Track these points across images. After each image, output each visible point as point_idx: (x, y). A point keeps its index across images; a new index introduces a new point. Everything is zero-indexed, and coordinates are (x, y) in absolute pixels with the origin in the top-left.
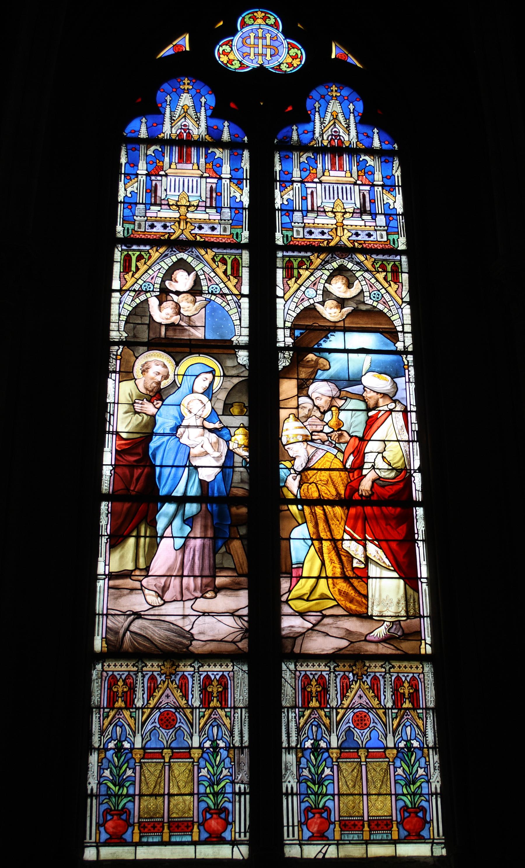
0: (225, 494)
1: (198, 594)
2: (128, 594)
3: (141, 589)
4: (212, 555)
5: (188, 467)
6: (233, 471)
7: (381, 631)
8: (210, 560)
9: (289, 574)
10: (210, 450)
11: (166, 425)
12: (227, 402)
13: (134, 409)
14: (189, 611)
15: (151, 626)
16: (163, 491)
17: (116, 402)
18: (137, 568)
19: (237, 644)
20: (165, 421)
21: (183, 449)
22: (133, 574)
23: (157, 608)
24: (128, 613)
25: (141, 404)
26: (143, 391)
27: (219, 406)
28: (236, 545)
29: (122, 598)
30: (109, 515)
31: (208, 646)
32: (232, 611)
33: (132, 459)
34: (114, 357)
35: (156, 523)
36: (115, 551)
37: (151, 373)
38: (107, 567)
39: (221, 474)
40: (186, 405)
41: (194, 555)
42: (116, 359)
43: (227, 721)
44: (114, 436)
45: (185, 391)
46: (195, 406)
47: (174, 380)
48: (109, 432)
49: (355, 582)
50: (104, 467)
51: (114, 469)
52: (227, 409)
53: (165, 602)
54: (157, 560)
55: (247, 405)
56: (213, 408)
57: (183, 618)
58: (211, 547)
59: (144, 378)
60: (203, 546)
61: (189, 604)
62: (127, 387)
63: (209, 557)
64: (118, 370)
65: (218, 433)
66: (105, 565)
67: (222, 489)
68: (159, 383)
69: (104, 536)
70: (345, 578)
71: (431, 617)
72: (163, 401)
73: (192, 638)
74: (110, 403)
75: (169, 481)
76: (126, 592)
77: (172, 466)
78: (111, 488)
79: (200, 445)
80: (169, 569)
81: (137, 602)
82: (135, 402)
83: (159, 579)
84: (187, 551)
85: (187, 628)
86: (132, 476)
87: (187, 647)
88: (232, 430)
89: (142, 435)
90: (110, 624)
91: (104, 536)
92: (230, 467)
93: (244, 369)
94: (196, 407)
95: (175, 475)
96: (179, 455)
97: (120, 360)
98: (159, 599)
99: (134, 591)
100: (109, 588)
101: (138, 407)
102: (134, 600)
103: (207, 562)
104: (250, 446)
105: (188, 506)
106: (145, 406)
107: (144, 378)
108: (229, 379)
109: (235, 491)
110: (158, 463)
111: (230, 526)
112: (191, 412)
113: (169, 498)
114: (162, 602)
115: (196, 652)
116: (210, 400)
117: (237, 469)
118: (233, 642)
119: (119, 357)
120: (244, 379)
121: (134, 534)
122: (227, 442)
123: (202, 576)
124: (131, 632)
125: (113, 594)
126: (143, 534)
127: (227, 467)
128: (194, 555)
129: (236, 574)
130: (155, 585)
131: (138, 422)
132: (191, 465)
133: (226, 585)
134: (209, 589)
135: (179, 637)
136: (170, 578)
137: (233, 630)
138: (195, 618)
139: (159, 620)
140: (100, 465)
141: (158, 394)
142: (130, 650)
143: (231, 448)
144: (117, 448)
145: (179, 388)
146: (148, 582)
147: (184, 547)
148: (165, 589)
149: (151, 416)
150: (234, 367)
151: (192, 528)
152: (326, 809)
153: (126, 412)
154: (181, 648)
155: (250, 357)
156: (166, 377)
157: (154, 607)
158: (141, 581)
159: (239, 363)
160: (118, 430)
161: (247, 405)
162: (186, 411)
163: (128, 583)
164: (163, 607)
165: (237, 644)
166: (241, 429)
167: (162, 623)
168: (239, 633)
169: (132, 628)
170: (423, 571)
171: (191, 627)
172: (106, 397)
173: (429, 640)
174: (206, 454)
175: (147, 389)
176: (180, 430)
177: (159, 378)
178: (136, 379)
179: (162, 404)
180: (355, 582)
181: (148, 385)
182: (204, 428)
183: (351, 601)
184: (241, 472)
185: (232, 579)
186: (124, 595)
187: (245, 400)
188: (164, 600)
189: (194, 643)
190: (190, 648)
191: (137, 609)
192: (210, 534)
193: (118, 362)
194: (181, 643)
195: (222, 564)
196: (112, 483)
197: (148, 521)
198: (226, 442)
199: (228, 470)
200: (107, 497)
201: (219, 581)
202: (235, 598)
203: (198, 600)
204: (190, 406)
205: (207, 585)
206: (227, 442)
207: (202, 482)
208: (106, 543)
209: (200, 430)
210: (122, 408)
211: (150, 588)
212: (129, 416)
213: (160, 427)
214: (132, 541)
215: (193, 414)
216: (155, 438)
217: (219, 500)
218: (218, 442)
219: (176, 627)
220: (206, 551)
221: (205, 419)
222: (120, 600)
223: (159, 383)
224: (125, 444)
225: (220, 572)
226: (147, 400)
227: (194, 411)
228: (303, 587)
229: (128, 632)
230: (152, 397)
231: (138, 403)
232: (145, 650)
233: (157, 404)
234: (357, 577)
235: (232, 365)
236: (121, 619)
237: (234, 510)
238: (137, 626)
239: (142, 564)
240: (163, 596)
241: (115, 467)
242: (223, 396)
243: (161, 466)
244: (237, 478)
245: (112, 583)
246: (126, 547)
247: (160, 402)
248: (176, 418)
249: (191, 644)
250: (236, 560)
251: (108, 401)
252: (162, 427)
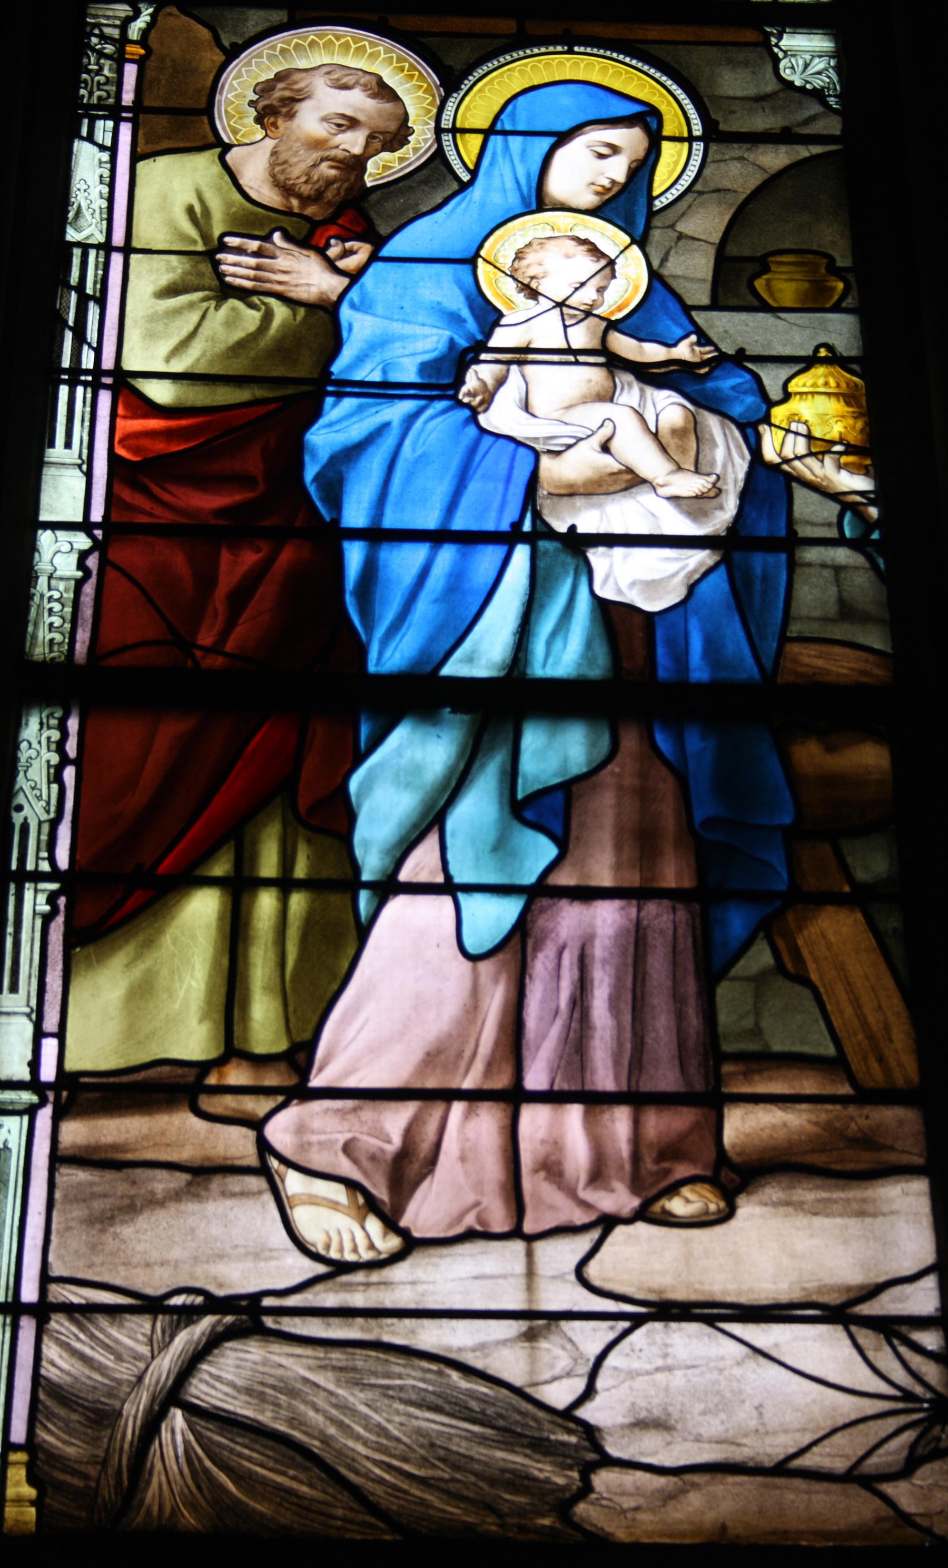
0: (748, 669)
1: (619, 1199)
2: (177, 1196)
3: (263, 1171)
4: (691, 986)
5: (531, 539)
6: (792, 565)
8: (680, 1016)
10: (649, 462)
11: (395, 350)
12: (732, 250)
13: (220, 276)
14: (561, 1295)
15: (324, 1379)
16: (390, 655)
17: (118, 238)
18: (232, 1049)
19: (889, 1489)
20: (392, 322)
21: (494, 460)
22: (212, 1080)
23: (359, 1277)
24: (178, 1300)
25: (257, 254)
26: (268, 195)
27: (694, 270)
28: (836, 937)
29: (143, 1221)
30: (69, 774)
31: (694, 1501)
32: (834, 1299)
33: (207, 502)
34: (109, 49)
35: (350, 817)
36: (101, 958)
37: (310, 121)
38: (50, 1046)
39: (720, 579)
40: (506, 261)
41: (583, 985)
42: (120, 61)
44: (105, 399)
45: (496, 199)
46: (560, 266)
47: (439, 155)
48: (75, 375)
50: (45, 538)
51: (97, 545)
52: (736, 282)
53: (411, 1245)
54: (355, 1009)
55: (843, 261)
56: (654, 275)
57: (530, 1336)
58: (686, 944)
59: (269, 144)
60: (637, 941)
61: (560, 1255)
62: (174, 187)
63: (678, 998)
64: (128, 98)
65: (691, 388)
66: (39, 1035)
67: (730, 649)
68: (356, 165)
69: (37, 877)
72: (378, 242)
73: (591, 1453)
74: (85, 247)
75: (424, 607)
76: (163, 1182)
77: (437, 537)
78: (83, 636)
79: (595, 441)
80: (433, 1058)
81: (236, 1244)
82: (223, 247)
83: (369, 1112)
84: (541, 965)
85: (559, 1395)
86: (206, 579)
87: (564, 1503)
88: (772, 378)
89: (260, 392)
90: (59, 1364)
91: (37, 877)
92: (770, 545)
93: (816, 108)
94: (561, 272)
95: (456, 583)
96: (474, 487)
97: (141, 62)
98: (374, 1225)
99: (216, 1183)
100: (57, 1159)
101: (237, 268)
102: (216, 1230)
103: (662, 1025)
104: (871, 448)
105: (533, 739)
106: (282, 262)
107: (269, 144)
108: (735, 150)
109: (809, 658)
110: (355, 514)
111: (792, 836)
112: (534, 294)
113: (422, 694)
114: (394, 1243)
115: (622, 1535)
116: (641, 242)
117: (812, 554)
118: (856, 1477)
119: (135, 51)
120: (816, 150)
121: (220, 868)
122: (750, 430)
123: (636, 1099)
124: (191, 1410)
125: (80, 1196)
126: (269, 867)
127: (757, 534)
128: (583, 985)
129: (845, 1089)
130: (348, 1148)
131: (239, 334)
132: (543, 532)
133: (790, 1147)
134: (682, 1171)
135: (509, 1447)
136: (437, 1110)
137: (850, 1407)
138: (603, 1333)
139: (373, 1348)
140: (26, 523)
141: (349, 211)
142: (189, 1518)
143: (770, 454)
144: (121, 451)
145: (465, 187)
146: (301, 1129)
147: (518, 945)
148: (409, 1167)
149: (312, 307)
150: (759, 99)
151: (563, 843)
153: (171, 291)
154: (521, 1512)
155: (844, 58)
156: (396, 137)
157: (340, 1268)
158: (257, 1125)
159: (790, 85)
160: (131, 363)
161: (843, 261)
162: (509, 286)
163: (183, 1132)
164: (399, 1272)
165: (889, 1489)
166: (820, 371)
167: (397, 1364)
168: (892, 1423)
169: (205, 1389)
171: (579, 1385)
172: (62, 223)
174: (631, 481)
175: (286, 190)
176: (479, 375)
177: (354, 142)
178: (227, 148)
179: (374, 258)
181: (296, 172)
182: (614, 363)
184: (838, 569)
185: (825, 1113)
186: (154, 1202)
187: (833, 238)
188: (404, 1234)
189: (603, 1479)
190: (581, 1508)
191: (239, 1279)
192: (673, 872)
193: (131, 71)
194: (519, 1481)
195: (756, 1032)
196: (87, 612)
197: (303, 803)
198: (742, 427)
199: (759, 561)
200: (56, 685)
201: (741, 1126)
202: (853, 1225)
203: (620, 1231)
204: (530, 267)
205: (671, 1151)
206: (750, 430)
207: (612, 617)
208: (47, 919)
209: (590, 376)
210: (148, 276)
211: (317, 1161)
212: (191, 306)
213: (361, 359)
214: (202, 908)
215: (545, 304)
216: (337, 410)
217: (716, 704)
218: (695, 428)
219: (483, 1389)
220: (658, 964)
221: (612, 325)
222: (126, 1231)
223: (356, 165)
224: (166, 434)
225: (747, 1076)
226: (287, 237)
227: (555, 287)
229: (178, 1417)
230: (315, 224)
231: (239, 251)
232: (286, 1518)
233: (346, 253)
235: (751, 92)
236: (133, 1334)
237: (810, 755)
238: (232, 1376)
239: (264, 1024)
240: (399, 1208)
241: (110, 535)
242: (708, 223)
243: (376, 536)
244: (813, 596)
245: (75, 1132)
246: (167, 940)
247: (363, 251)
248: (454, 319)
249: (586, 1489)
250: (844, 1014)
251: (72, 235)
252: (378, 357)
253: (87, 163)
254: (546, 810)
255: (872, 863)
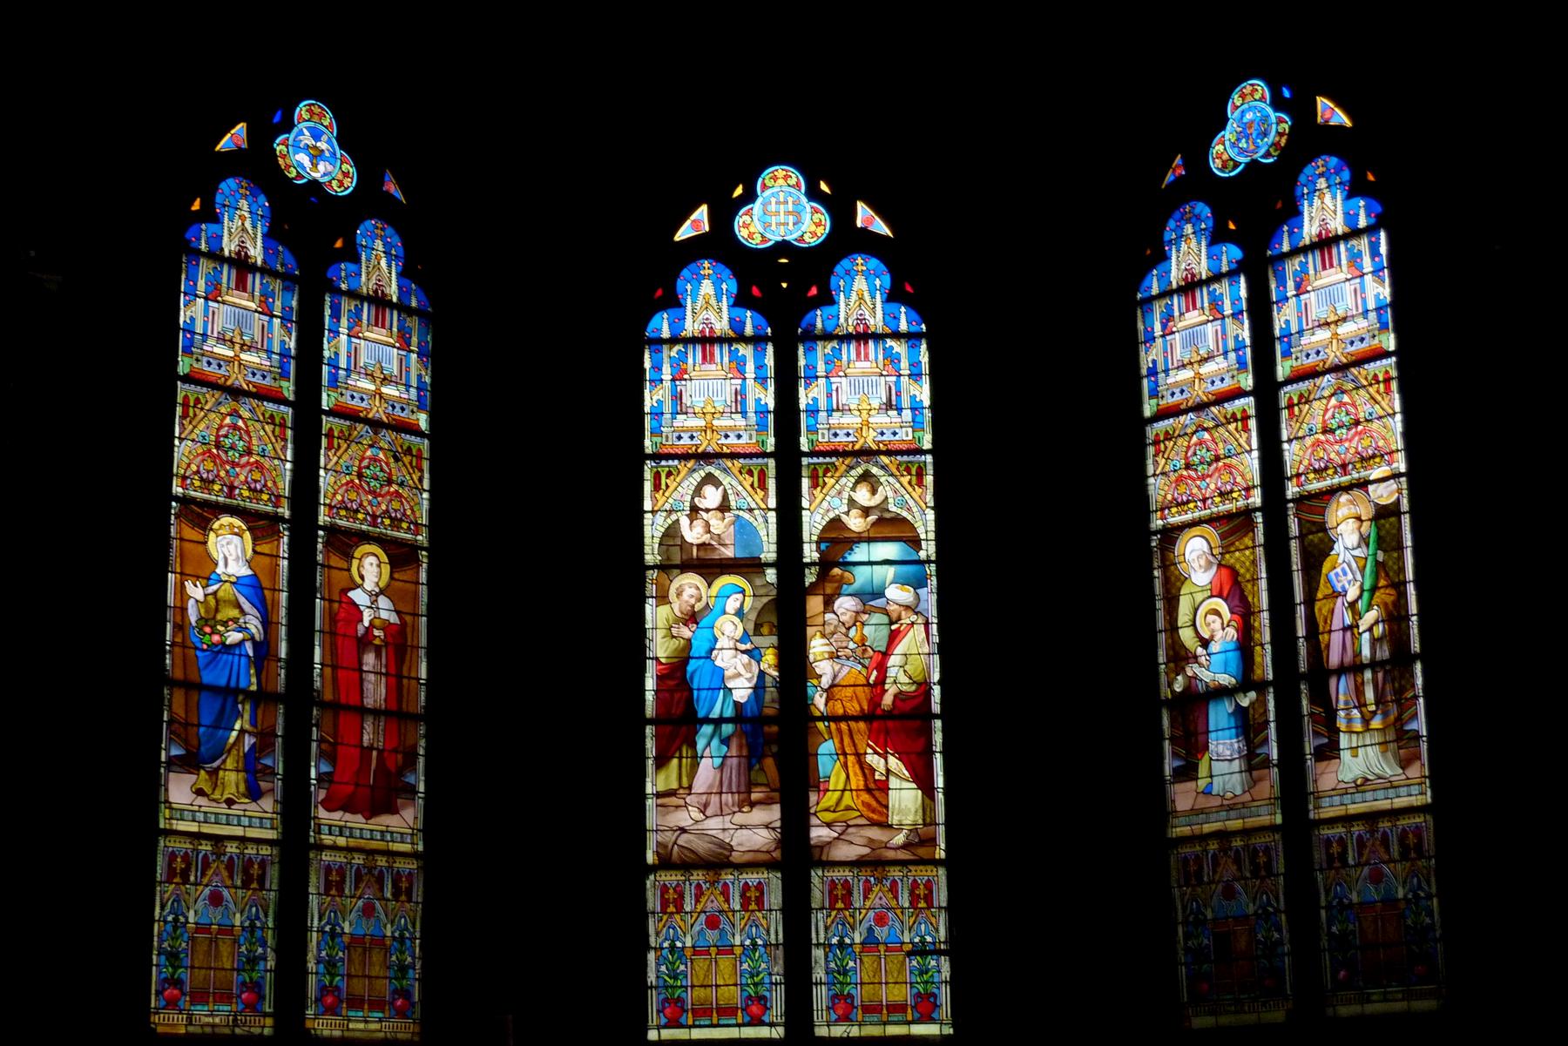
7: (900, 839)
9: (817, 787)
10: (742, 671)
14: (729, 825)
16: (701, 714)
18: (681, 787)
27: (751, 626)
28: (769, 763)
37: (685, 596)
43: (764, 922)
46: (728, 628)
49: (877, 793)
52: (757, 630)
60: (739, 764)
62: (664, 611)
70: (868, 790)
71: (947, 824)
73: (732, 849)
81: (682, 818)
94: (728, 628)
101: (674, 631)
139: (702, 834)
141: (692, 618)
147: (722, 766)
148: (706, 805)
152: (337, 988)
170: (940, 782)
173: (943, 846)
174: (739, 675)
177: (693, 601)
180: (877, 793)
183: (873, 811)
191: (682, 824)
200: (651, 722)
201: (754, 796)
207: (736, 703)
214: (675, 762)
216: (692, 662)
228: (830, 799)
234: (878, 789)
242: (753, 616)
245: (660, 801)
253: (648, 609)
254: (726, 741)
255: (775, 749)
